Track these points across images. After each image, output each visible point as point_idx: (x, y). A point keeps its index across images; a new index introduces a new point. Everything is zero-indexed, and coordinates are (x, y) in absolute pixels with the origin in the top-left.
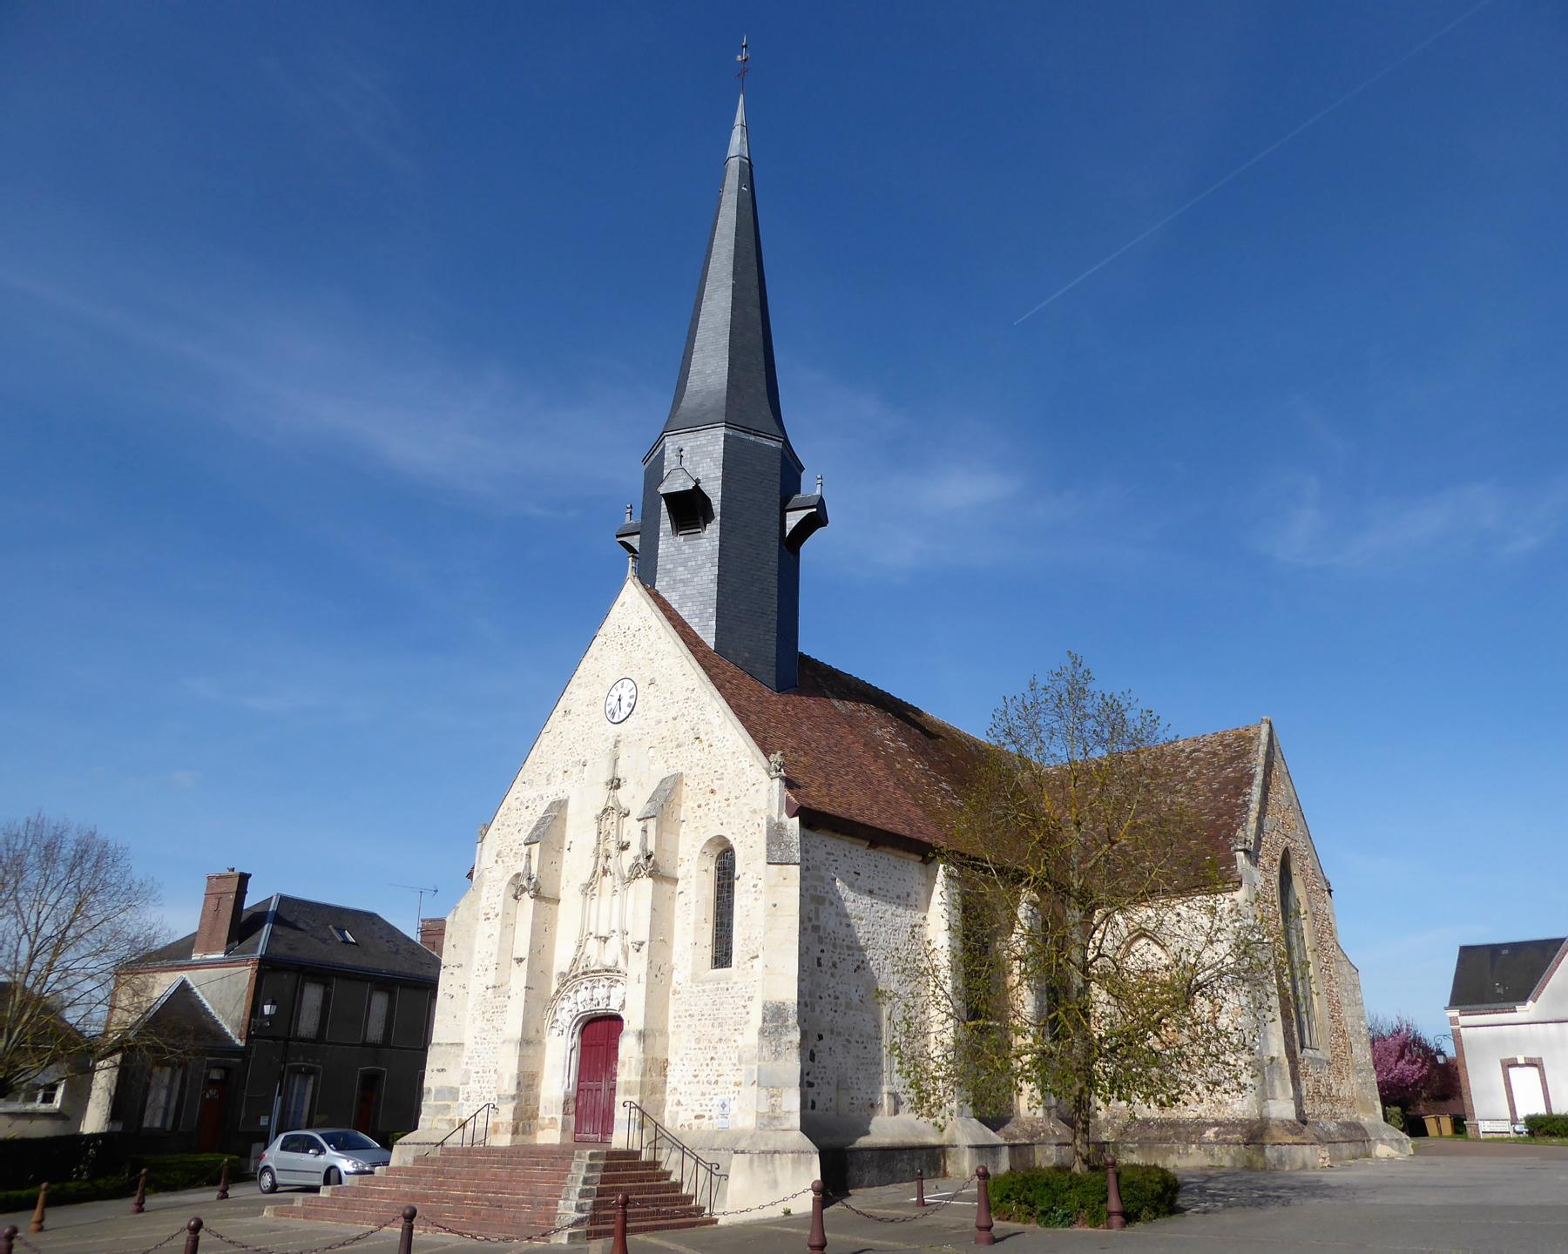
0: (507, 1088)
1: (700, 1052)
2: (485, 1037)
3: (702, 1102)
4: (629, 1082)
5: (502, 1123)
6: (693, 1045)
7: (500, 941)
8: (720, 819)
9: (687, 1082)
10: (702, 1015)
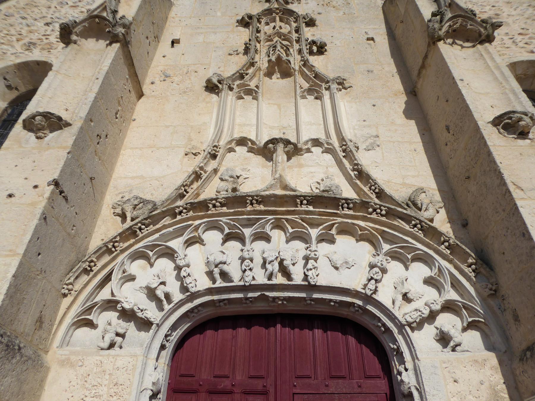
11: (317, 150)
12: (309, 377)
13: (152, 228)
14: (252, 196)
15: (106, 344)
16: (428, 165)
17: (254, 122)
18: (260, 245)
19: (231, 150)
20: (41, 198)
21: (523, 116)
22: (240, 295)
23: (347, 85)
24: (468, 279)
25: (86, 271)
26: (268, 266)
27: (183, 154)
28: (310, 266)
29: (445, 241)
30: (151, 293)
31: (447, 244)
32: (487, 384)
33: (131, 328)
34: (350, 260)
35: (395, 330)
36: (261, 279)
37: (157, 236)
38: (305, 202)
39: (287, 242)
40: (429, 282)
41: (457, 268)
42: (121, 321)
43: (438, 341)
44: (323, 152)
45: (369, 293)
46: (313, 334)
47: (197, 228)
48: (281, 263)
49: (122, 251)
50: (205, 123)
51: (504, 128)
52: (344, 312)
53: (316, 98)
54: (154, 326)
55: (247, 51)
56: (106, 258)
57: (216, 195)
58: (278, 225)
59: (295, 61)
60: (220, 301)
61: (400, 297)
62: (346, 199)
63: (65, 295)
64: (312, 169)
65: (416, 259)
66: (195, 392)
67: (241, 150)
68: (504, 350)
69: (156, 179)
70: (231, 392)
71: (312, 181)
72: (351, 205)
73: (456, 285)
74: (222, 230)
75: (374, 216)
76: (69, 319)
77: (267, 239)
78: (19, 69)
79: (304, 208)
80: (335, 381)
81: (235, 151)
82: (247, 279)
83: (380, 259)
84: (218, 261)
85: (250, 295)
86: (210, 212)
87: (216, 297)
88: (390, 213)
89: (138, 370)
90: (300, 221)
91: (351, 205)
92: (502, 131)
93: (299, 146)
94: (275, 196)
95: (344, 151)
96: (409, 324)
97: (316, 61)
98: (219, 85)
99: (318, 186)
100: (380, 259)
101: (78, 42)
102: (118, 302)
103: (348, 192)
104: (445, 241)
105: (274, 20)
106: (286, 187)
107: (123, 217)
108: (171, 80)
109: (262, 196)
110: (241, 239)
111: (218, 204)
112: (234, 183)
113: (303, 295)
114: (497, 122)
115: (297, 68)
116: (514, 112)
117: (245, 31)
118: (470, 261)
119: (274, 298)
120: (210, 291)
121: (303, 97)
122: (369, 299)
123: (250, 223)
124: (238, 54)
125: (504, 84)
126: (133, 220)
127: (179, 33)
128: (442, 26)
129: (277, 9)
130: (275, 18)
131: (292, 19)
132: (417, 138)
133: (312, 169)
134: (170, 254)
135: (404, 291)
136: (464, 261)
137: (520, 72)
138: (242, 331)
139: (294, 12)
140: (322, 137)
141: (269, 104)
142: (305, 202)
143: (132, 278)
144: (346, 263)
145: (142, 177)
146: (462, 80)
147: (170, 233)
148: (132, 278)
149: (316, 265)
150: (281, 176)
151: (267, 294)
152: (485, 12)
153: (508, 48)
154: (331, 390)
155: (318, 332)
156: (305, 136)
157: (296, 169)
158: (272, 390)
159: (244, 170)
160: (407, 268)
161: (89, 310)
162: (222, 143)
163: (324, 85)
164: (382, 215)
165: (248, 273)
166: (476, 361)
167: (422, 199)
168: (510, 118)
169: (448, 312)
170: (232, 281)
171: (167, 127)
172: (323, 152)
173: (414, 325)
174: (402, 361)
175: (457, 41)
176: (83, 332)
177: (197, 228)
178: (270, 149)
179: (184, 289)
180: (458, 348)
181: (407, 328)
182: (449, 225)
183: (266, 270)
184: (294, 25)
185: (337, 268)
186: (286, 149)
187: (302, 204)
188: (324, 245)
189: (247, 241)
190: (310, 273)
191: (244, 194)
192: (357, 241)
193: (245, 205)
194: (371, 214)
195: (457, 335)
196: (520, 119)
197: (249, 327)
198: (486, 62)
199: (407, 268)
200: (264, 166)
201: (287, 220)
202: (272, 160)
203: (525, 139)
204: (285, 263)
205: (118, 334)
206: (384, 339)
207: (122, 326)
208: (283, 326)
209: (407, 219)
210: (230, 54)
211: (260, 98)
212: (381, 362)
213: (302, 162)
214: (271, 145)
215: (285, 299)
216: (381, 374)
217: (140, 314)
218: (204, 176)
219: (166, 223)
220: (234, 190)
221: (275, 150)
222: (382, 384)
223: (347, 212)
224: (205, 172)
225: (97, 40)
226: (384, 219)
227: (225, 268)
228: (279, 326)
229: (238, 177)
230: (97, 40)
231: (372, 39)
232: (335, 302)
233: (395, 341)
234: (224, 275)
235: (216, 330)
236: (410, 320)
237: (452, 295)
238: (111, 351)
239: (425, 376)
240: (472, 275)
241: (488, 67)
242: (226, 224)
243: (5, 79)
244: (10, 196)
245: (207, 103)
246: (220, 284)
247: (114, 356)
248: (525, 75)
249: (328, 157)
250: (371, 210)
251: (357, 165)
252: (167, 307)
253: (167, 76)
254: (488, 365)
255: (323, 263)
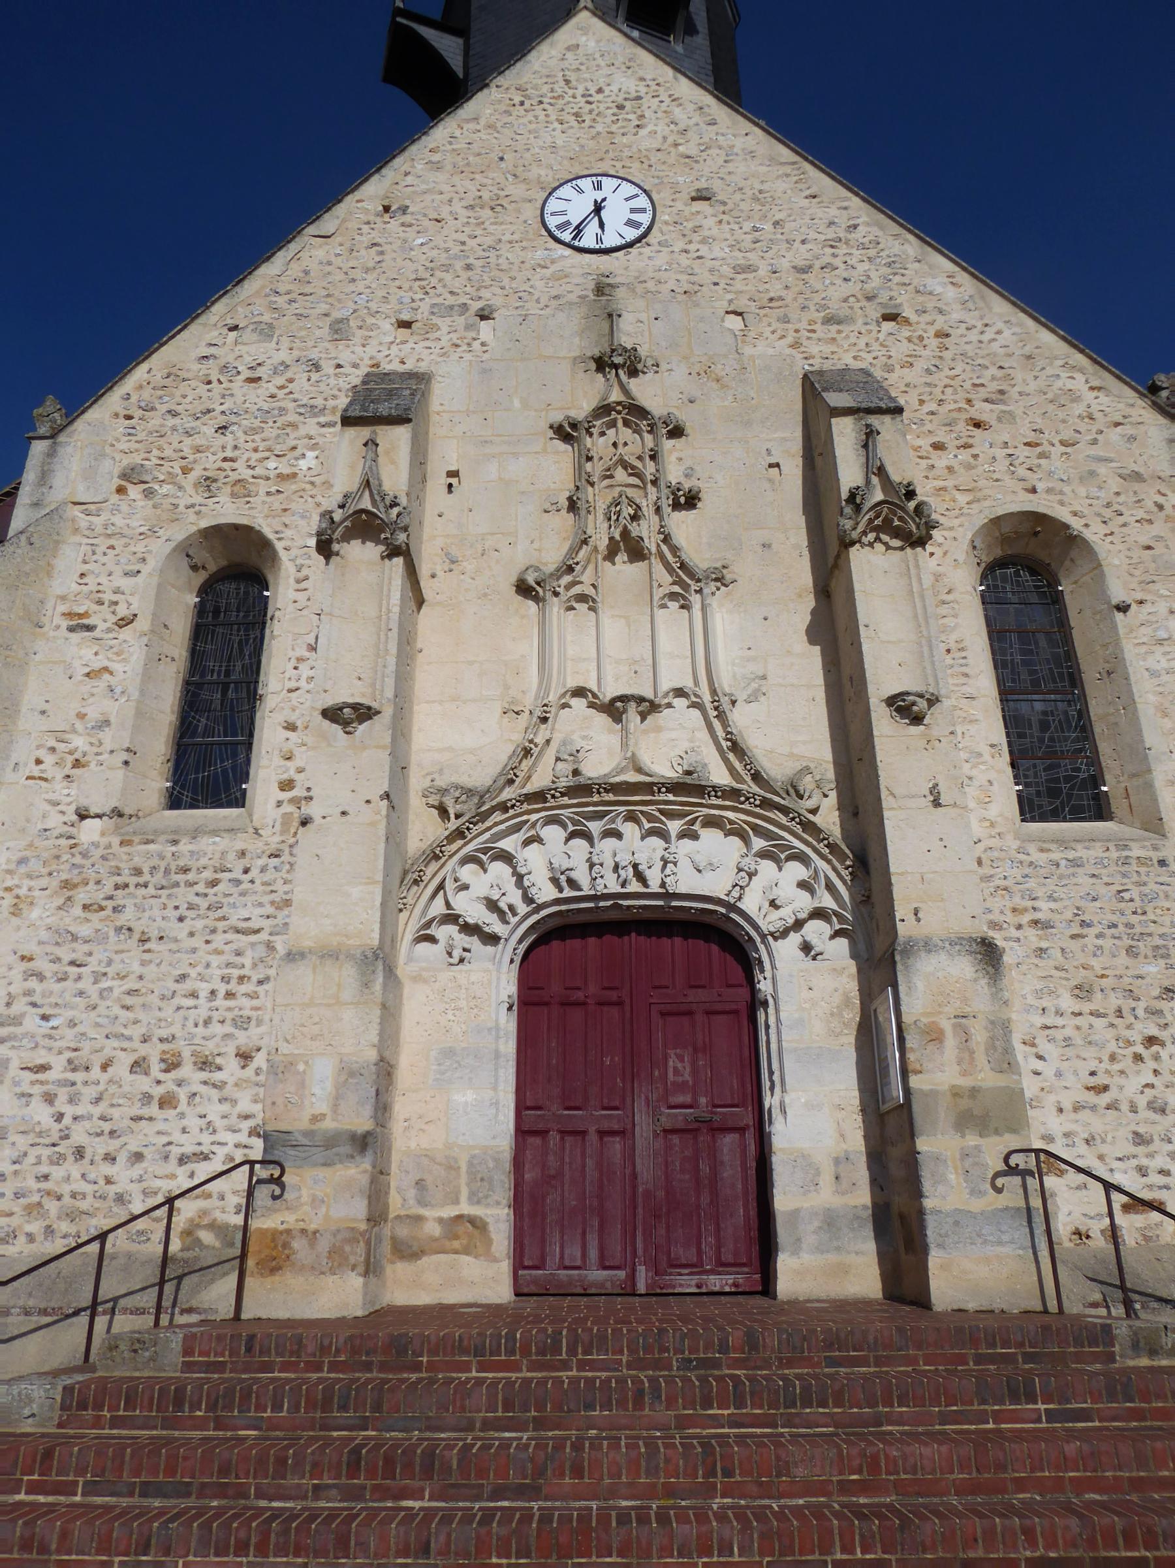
0: (323, 1107)
1: (1099, 1023)
2: (79, 956)
3: (1145, 1162)
4: (974, 1092)
5: (312, 1236)
6: (1067, 1002)
7: (142, 692)
8: (131, 816)
9: (1067, 1105)
10: (1083, 924)
11: (680, 703)
12: (667, 987)
13: (481, 827)
14: (599, 785)
15: (455, 960)
16: (827, 723)
17: (593, 653)
18: (611, 843)
19: (565, 706)
20: (378, 817)
21: (918, 699)
22: (592, 905)
23: (729, 577)
24: (844, 882)
25: (416, 882)
26: (622, 872)
27: (500, 711)
28: (668, 871)
29: (824, 839)
30: (492, 905)
31: (826, 842)
32: (841, 991)
33: (474, 942)
34: (714, 861)
35: (758, 940)
36: (614, 888)
37: (487, 835)
38: (664, 790)
39: (643, 838)
40: (803, 885)
41: (834, 869)
42: (462, 935)
43: (802, 949)
44: (688, 707)
45: (732, 901)
46: (673, 945)
47: (534, 825)
48: (635, 866)
49: (451, 856)
50: (523, 656)
51: (897, 710)
52: (707, 919)
53: (682, 607)
54: (502, 941)
55: (573, 506)
56: (434, 866)
57: (553, 782)
58: (631, 817)
59: (647, 531)
60: (568, 911)
61: (767, 904)
62: (714, 787)
63: (401, 910)
64: (673, 735)
65: (789, 858)
66: (547, 1004)
67: (579, 704)
68: (866, 957)
69: (471, 753)
70: (584, 1004)
71: (672, 754)
72: (719, 794)
73: (830, 887)
74: (564, 827)
75: (746, 806)
76: (409, 936)
77: (618, 835)
78: (206, 537)
79: (662, 797)
80: (694, 990)
81: (570, 707)
82: (598, 888)
83: (749, 863)
84: (564, 868)
85: (602, 904)
86: (548, 805)
87: (563, 908)
88: (766, 804)
89: (494, 984)
90: (658, 814)
91: (719, 794)
92: (894, 713)
93: (657, 701)
94: (626, 783)
95: (716, 708)
96: (772, 934)
97: (682, 524)
98: (538, 589)
99: (680, 761)
100: (749, 863)
101: (342, 552)
102: (459, 916)
103: (719, 776)
104: (824, 839)
105: (613, 424)
106: (639, 770)
107: (443, 812)
108: (461, 568)
109: (611, 784)
110: (587, 836)
111: (558, 794)
112: (574, 762)
113: (661, 903)
114: (891, 701)
115: (654, 550)
116: (908, 694)
117: (566, 451)
118: (848, 863)
119: (628, 907)
120: (557, 902)
121: (664, 606)
122: (732, 907)
123: (599, 816)
124: (558, 511)
125: (923, 629)
126: (457, 817)
127: (455, 456)
128: (857, 524)
129: (619, 403)
130: (615, 420)
131: (644, 424)
132: (819, 679)
133: (673, 735)
134: (506, 857)
135: (771, 898)
136: (842, 862)
137: (1007, 530)
138: (592, 941)
139: (648, 413)
140: (687, 683)
141: (613, 616)
142: (664, 790)
143: (465, 887)
144: (711, 864)
145: (450, 749)
146: (866, 626)
147: (503, 831)
148: (465, 887)
149: (675, 870)
150: (633, 754)
151: (620, 902)
152: (983, 385)
153: (997, 480)
154: (689, 999)
155: (678, 941)
156: (665, 685)
157: (652, 735)
158: (627, 1001)
159: (584, 738)
160: (780, 869)
161: (428, 924)
162: (552, 698)
163: (694, 586)
164: (756, 806)
165: (599, 881)
166: (835, 969)
167: (807, 783)
168: (904, 700)
169: (818, 919)
170: (581, 890)
171: (471, 663)
172: (688, 707)
173: (777, 934)
174: (762, 971)
175: (882, 536)
176: (425, 946)
177: (534, 825)
178: (617, 708)
179: (528, 899)
180: (819, 957)
181: (770, 938)
182: (837, 813)
183: (619, 876)
184: (648, 438)
185: (699, 871)
186: (640, 709)
187: (659, 792)
188: (686, 841)
189: (596, 841)
190: (668, 880)
191: (590, 782)
192: (726, 835)
193: (591, 795)
194: (742, 803)
195: (818, 944)
196: (914, 704)
197: (600, 936)
198: (910, 584)
199: (780, 869)
200: (610, 731)
201: (642, 812)
202: (621, 721)
203: (919, 725)
204: (640, 867)
205: (465, 950)
206: (747, 946)
207: (462, 940)
208: (639, 934)
209: (785, 810)
210: (546, 511)
211: (600, 611)
212: (744, 970)
213: (661, 722)
214: (619, 704)
215: (640, 907)
216: (745, 983)
217: (487, 929)
218: (535, 751)
219: (497, 820)
220: (576, 773)
221: (625, 711)
222: (744, 992)
223: (715, 801)
224: (536, 746)
225: (363, 543)
226: (758, 810)
227: (573, 874)
228: (633, 934)
229: (578, 751)
230: (363, 543)
231: (777, 465)
232: (696, 909)
233: (757, 950)
234: (572, 883)
235: (563, 940)
236: (772, 929)
237: (828, 902)
238: (460, 967)
239: (780, 984)
240: (848, 878)
241: (911, 591)
242: (569, 818)
243: (188, 556)
244: (344, 813)
245: (523, 617)
246: (568, 893)
247: (466, 972)
248: (1016, 533)
249: (696, 713)
250: (742, 799)
251: (731, 733)
252: (514, 920)
253: (453, 562)
254: (847, 973)
255: (685, 867)
